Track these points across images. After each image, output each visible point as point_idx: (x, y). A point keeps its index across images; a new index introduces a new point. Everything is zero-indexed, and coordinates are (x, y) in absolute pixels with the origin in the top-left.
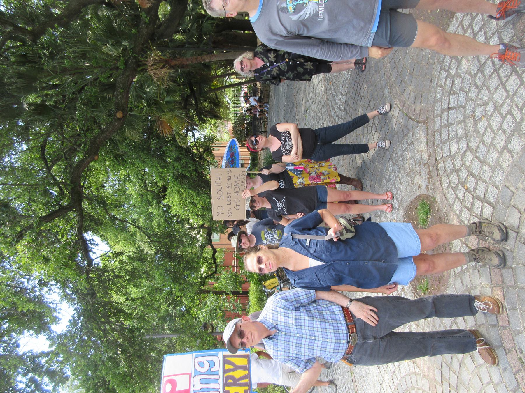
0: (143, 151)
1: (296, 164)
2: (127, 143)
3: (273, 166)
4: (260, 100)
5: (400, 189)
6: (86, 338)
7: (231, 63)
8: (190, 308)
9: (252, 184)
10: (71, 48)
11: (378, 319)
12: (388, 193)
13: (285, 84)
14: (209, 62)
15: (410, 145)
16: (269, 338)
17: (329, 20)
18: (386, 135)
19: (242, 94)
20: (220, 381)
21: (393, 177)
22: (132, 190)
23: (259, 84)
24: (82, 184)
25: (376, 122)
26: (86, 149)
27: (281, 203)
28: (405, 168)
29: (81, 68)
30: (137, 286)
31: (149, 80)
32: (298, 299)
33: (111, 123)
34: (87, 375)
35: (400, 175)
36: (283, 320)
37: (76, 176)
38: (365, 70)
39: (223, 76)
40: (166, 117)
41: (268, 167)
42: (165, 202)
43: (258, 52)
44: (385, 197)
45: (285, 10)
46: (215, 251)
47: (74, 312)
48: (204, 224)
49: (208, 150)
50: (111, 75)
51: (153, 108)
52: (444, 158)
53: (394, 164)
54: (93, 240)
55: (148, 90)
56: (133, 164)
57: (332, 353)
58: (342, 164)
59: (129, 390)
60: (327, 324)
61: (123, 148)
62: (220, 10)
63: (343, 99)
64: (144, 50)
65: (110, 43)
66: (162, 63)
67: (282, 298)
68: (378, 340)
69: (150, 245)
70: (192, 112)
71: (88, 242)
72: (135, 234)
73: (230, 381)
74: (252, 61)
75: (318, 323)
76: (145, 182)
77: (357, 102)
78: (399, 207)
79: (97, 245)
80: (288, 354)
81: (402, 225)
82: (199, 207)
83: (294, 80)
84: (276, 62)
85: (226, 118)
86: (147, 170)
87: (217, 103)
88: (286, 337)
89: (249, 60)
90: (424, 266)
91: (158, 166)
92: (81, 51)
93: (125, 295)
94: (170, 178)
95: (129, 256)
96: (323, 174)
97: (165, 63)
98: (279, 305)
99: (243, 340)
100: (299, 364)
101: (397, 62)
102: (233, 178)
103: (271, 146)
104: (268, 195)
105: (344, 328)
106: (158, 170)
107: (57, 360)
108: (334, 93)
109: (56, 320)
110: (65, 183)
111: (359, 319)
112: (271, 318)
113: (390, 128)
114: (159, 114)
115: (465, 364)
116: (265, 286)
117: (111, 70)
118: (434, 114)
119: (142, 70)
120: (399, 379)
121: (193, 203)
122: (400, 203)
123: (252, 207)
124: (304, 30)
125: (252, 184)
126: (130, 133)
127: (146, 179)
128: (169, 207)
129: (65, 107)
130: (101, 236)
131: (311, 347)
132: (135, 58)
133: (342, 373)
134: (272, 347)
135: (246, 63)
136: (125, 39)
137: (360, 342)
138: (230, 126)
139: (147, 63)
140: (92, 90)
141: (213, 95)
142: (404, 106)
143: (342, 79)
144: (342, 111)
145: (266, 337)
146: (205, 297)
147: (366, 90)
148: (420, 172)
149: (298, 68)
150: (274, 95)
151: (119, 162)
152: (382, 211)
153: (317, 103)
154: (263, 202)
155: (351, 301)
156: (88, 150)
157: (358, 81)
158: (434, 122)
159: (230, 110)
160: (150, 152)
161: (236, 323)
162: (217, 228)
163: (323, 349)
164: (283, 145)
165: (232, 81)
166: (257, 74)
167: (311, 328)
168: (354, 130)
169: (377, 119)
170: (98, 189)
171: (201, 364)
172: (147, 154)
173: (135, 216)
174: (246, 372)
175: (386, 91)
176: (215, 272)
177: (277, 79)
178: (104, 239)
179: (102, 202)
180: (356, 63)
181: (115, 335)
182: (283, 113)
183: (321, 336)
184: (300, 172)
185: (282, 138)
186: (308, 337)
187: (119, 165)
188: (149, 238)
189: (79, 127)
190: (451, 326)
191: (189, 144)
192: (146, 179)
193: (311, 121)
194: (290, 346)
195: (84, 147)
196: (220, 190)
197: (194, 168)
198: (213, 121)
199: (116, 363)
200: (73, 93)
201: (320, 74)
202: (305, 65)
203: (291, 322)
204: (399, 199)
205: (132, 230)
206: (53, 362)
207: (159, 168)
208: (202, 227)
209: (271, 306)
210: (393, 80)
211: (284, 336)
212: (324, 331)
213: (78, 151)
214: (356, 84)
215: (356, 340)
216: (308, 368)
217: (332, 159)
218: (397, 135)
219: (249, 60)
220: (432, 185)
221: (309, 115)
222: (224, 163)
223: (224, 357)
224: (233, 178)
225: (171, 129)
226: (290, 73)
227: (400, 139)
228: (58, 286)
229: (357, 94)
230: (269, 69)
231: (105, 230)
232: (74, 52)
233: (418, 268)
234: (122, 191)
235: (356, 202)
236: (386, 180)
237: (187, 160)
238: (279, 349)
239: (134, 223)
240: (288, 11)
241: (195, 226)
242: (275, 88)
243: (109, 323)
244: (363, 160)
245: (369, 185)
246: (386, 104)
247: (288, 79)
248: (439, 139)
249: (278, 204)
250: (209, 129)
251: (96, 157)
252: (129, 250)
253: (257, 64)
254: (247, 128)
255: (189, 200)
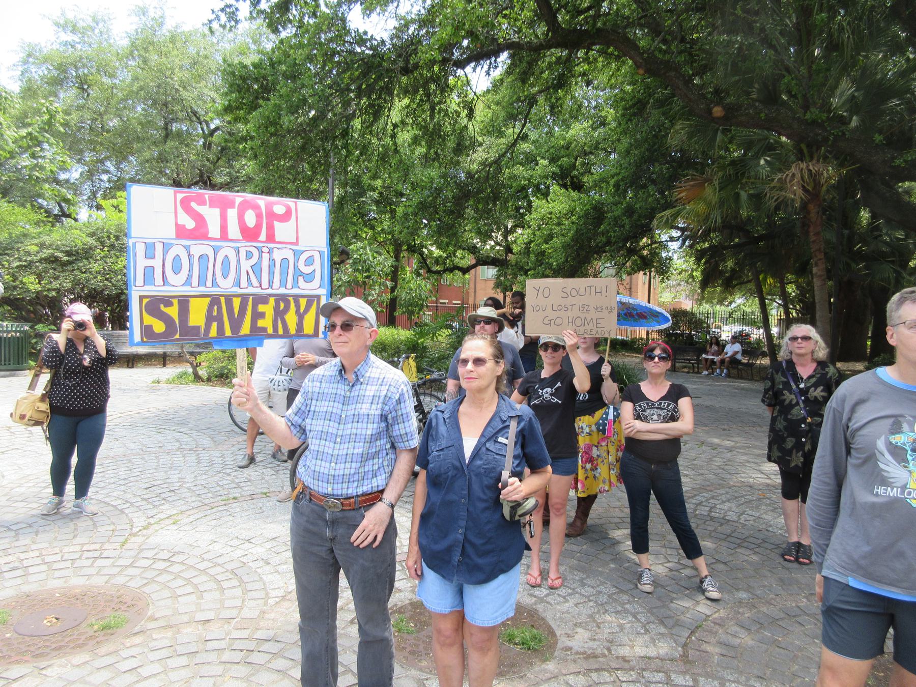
0: (647, 150)
1: (617, 423)
2: (664, 123)
3: (615, 385)
4: (733, 361)
5: (567, 601)
6: (336, 59)
7: (808, 316)
8: (372, 228)
9: (584, 346)
10: (848, 24)
11: (361, 546)
12: (559, 581)
13: (766, 413)
14: (811, 272)
15: (644, 626)
16: (341, 370)
17: (873, 505)
18: (663, 587)
19: (747, 329)
20: (283, 291)
21: (587, 591)
22: (578, 130)
23: (766, 361)
24: (594, 47)
25: (688, 572)
26: (657, 53)
27: (551, 395)
28: (604, 613)
29: (809, 41)
30: (416, 141)
31: (780, 164)
32: (400, 420)
33: (703, 96)
34: (280, 63)
35: (591, 604)
36: (367, 393)
37: (608, 37)
38: (786, 560)
39: (784, 295)
40: (711, 193)
41: (615, 375)
42: (555, 188)
43: (827, 370)
44: (553, 575)
45: (896, 429)
46: (465, 271)
47: (379, 39)
48: (512, 253)
49: (645, 264)
50: (795, 96)
51: (730, 171)
52: (618, 683)
53: (610, 596)
54: (496, 67)
55: (762, 162)
56: (625, 132)
57: (313, 468)
58: (613, 503)
59: (254, 131)
60: (358, 465)
61: (654, 116)
62: (899, 317)
63: (732, 516)
64: (841, 157)
65: (856, 94)
66: (813, 189)
67: (402, 395)
68: (328, 544)
69: (484, 164)
70: (715, 238)
71: (493, 59)
72: (501, 134)
73: (282, 306)
74: (809, 357)
75: (361, 450)
76: (591, 153)
77: (725, 540)
78: (535, 596)
79: (488, 74)
80: (315, 397)
81: (512, 602)
82: (545, 246)
83: (770, 431)
84: (807, 401)
85: (703, 298)
86: (612, 156)
87: (731, 284)
88: (342, 398)
89: (813, 352)
90: (447, 626)
91: (620, 177)
92: (843, 43)
93: (403, 122)
94: (597, 197)
95: (466, 127)
96: (595, 468)
97: (813, 190)
98: (392, 389)
99: (338, 328)
100: (299, 415)
101: (799, 619)
102: (599, 315)
103: (651, 383)
104: (565, 374)
105: (350, 491)
106: (613, 177)
107: (304, 15)
108: (743, 500)
109: (368, 11)
110: (598, 16)
111: (364, 517)
112: (372, 375)
113: (675, 595)
114: (716, 183)
115: (281, 680)
116: (408, 358)
117: (804, 96)
118: (699, 675)
119: (801, 151)
120: (258, 570)
121: (550, 237)
122: (541, 600)
123: (546, 346)
124: (859, 458)
125: (584, 346)
126: (683, 129)
127: (597, 156)
128: (546, 194)
129: (735, 14)
130: (501, 80)
131: (324, 436)
132: (826, 140)
133: (267, 478)
134: (327, 373)
135: (806, 347)
136: (862, 121)
137: (328, 515)
138: (687, 305)
139: (814, 162)
140: (766, 63)
141: (748, 276)
142: (715, 623)
143: (768, 517)
144: (710, 511)
145: (343, 366)
146: (388, 252)
147: (746, 558)
148: (595, 640)
149: (794, 440)
150: (743, 389)
151: (631, 107)
152: (528, 566)
153: (726, 467)
154: (553, 365)
155: (392, 506)
156: (656, 57)
157: (766, 545)
158: (684, 673)
159: (718, 307)
160: (645, 162)
161: (366, 319)
162: (505, 277)
163: (319, 455)
164: (653, 405)
165: (774, 312)
166: (784, 365)
167: (353, 438)
168: (674, 530)
169: (693, 572)
170: (584, 74)
171: (309, 261)
172: (643, 157)
173: (533, 136)
174: (293, 331)
175: (743, 595)
176: (429, 271)
177: (774, 398)
178: (496, 86)
179: (562, 82)
180: (799, 545)
181: (339, 109)
182: (708, 403)
183: (341, 453)
184: (602, 429)
185: (665, 404)
186: (340, 433)
187: (625, 109)
188: (495, 162)
189: (698, 38)
190: (343, 665)
191: (657, 232)
192: (597, 156)
193: (693, 454)
194: (327, 403)
195: (661, 50)
196: (578, 292)
197: (613, 240)
198: (697, 274)
199: (293, 110)
200: (763, 30)
201: (779, 477)
202: (798, 452)
203: (364, 406)
204: (549, 599)
205: (511, 130)
206: (301, 7)
207: (616, 178)
208: (508, 250)
209: (392, 376)
210: (764, 609)
211: (343, 393)
212: (347, 458)
213: (653, 40)
214: (759, 541)
215: (332, 510)
216: (292, 428)
217: (623, 487)
218: (663, 606)
219: (813, 352)
220: (572, 657)
221: (704, 452)
222: (625, 299)
223: (318, 297)
224: (599, 315)
225: (686, 201)
226: (785, 424)
227: (655, 610)
228: (423, 11)
229: (739, 541)
230: (793, 385)
231: (512, 86)
232: (841, 29)
233: (443, 616)
234: (576, 114)
235: (546, 523)
236: (583, 579)
237: (627, 227)
238: (324, 385)
239: (524, 137)
240: (893, 434)
241: (509, 239)
242: (757, 391)
243: (359, 97)
244: (618, 543)
245: (575, 548)
246: (720, 592)
247: (774, 420)
248: (654, 680)
249: (549, 390)
250: (684, 267)
251: (641, 71)
252: (474, 128)
253: (802, 365)
254: (682, 335)
255: (557, 229)
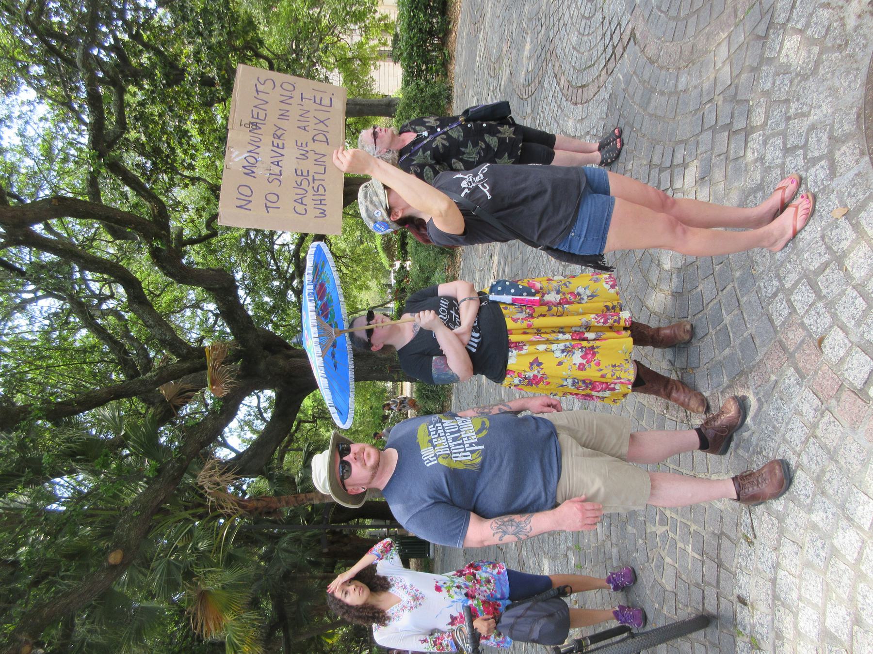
202: (499, 132)
